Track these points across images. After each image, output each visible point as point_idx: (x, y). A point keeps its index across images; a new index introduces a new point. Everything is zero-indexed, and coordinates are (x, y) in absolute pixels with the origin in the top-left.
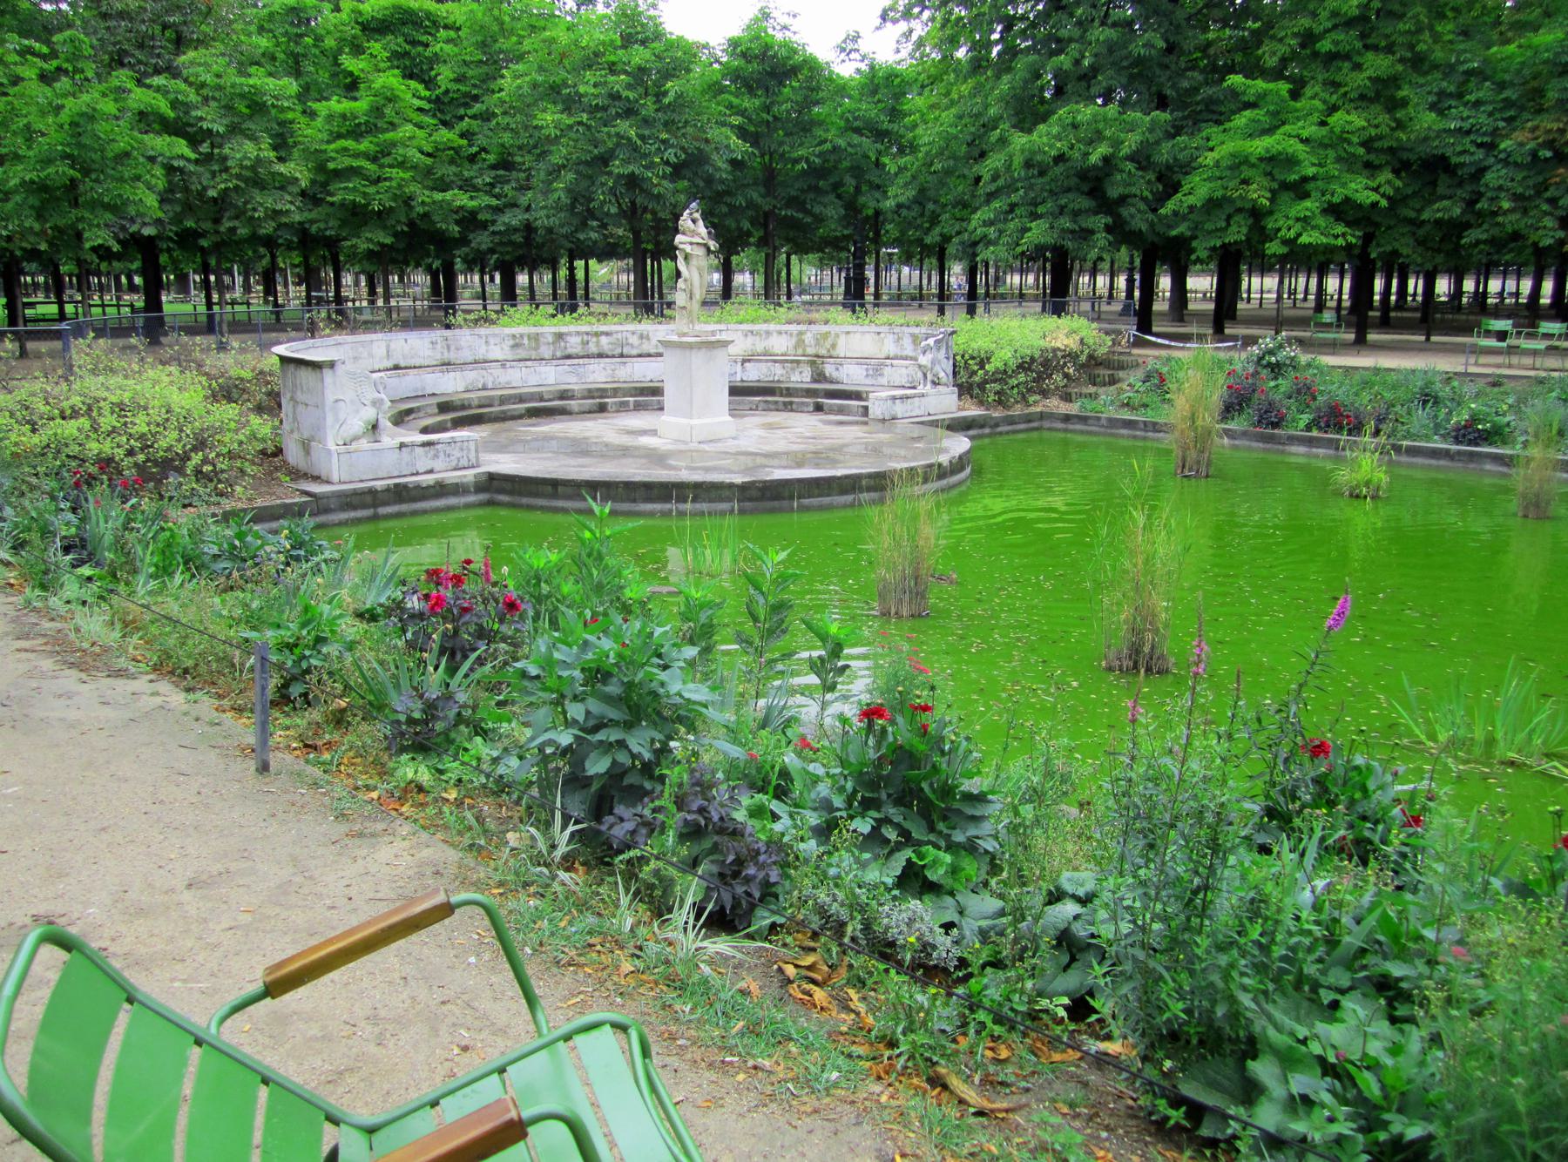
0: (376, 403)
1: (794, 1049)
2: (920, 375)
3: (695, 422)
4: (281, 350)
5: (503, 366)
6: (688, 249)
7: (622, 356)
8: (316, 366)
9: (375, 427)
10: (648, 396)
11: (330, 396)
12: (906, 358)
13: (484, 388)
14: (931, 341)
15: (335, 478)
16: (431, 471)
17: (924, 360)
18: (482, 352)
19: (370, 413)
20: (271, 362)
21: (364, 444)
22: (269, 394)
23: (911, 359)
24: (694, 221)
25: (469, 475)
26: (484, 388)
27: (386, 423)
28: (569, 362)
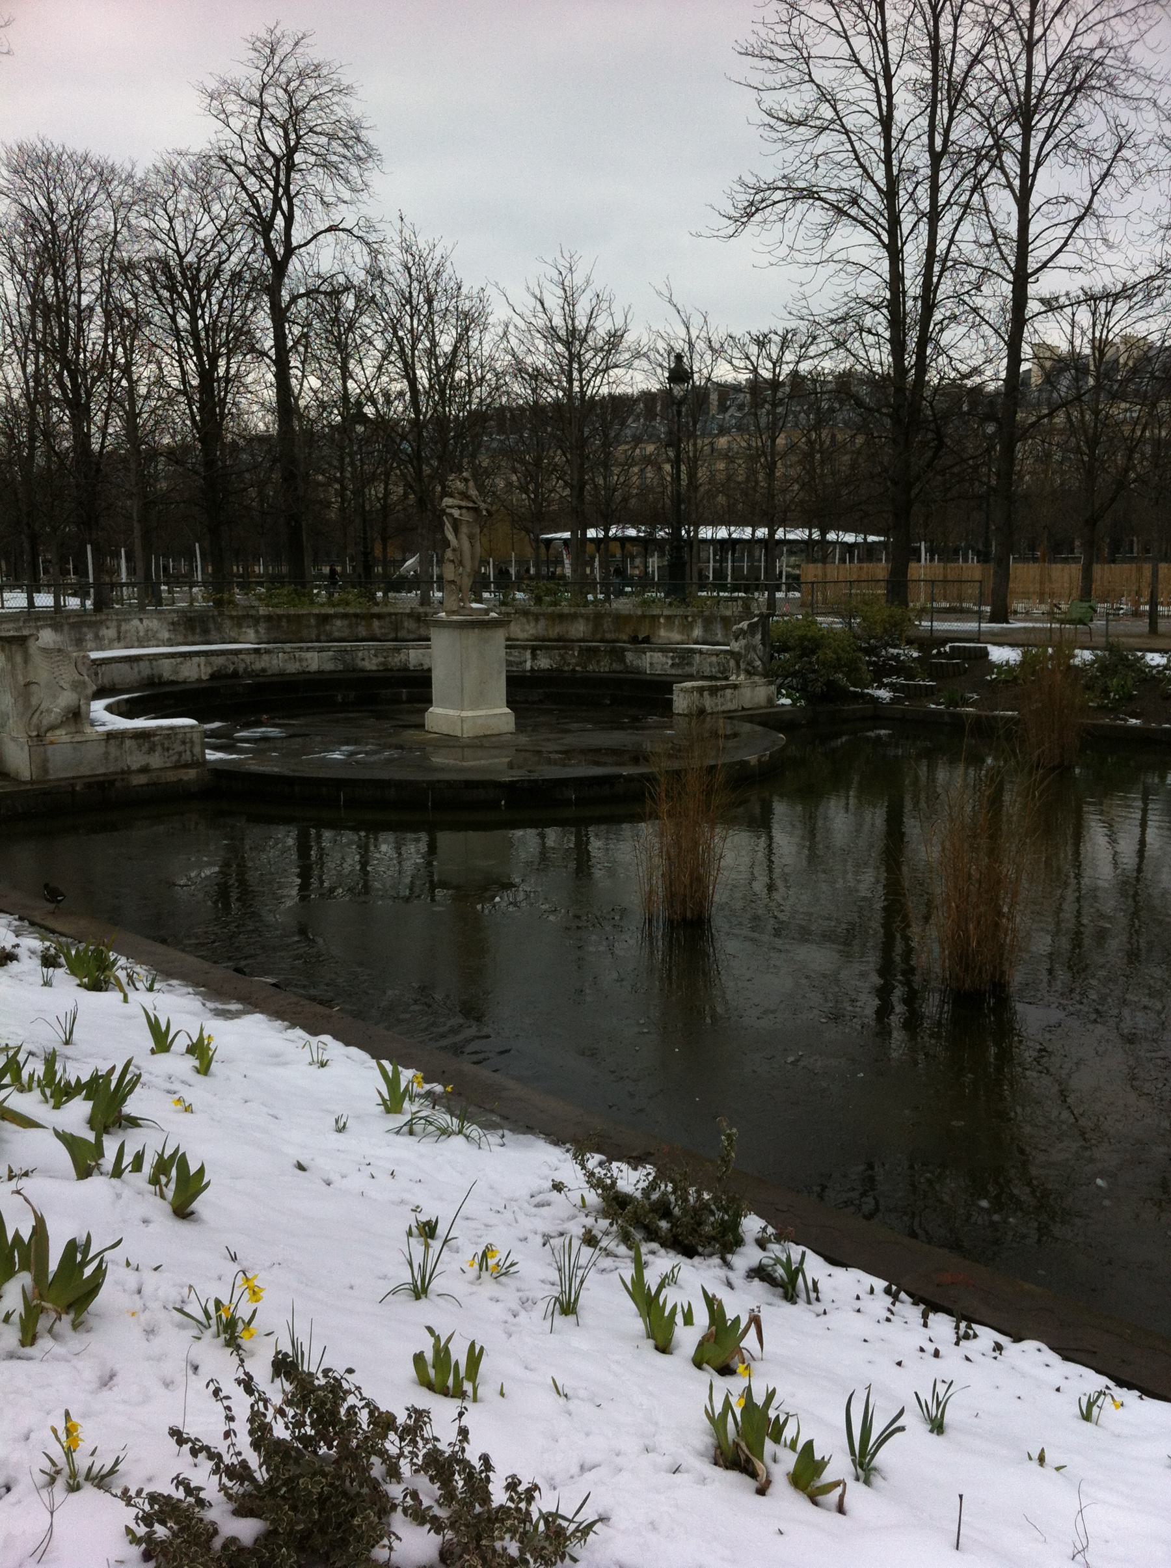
2: (732, 663)
3: (465, 714)
6: (456, 513)
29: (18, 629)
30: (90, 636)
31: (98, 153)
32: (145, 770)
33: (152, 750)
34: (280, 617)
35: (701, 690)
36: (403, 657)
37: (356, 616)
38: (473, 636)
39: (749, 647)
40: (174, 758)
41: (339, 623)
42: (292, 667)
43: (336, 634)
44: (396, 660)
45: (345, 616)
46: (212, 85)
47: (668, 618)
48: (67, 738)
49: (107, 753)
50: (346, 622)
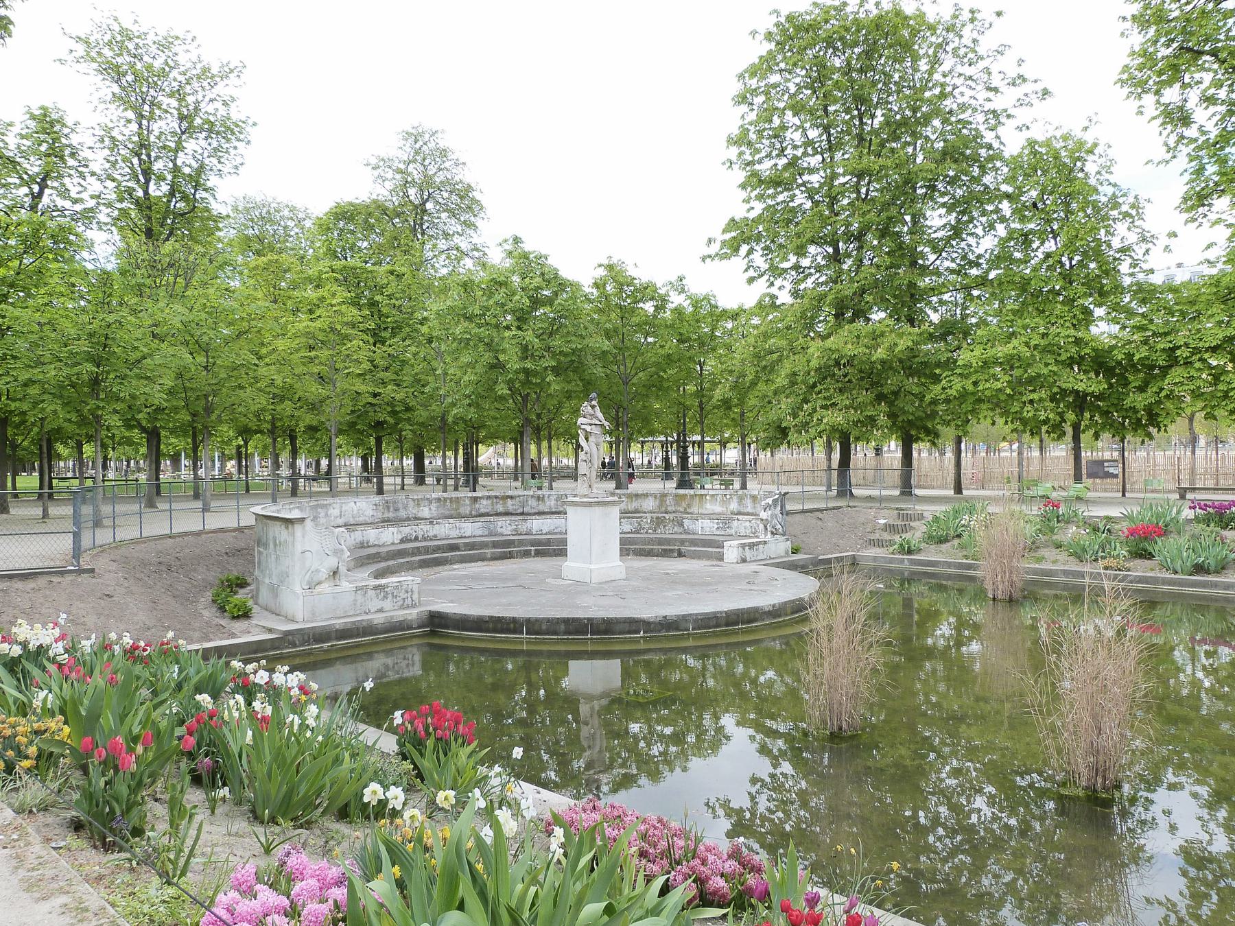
0: (338, 552)
1: (235, 284)
2: (761, 526)
3: (592, 567)
4: (258, 509)
5: (431, 523)
6: (588, 428)
7: (522, 514)
8: (288, 522)
9: (335, 573)
10: (553, 548)
11: (299, 548)
12: (748, 514)
13: (416, 539)
14: (770, 501)
15: (300, 617)
16: (381, 610)
17: (764, 515)
18: (413, 511)
19: (332, 562)
20: (248, 520)
21: (326, 588)
22: (1043, 311)
23: (752, 514)
24: (593, 407)
25: (412, 614)
26: (425, 539)
27: (343, 569)
28: (483, 519)
29: (278, 511)
30: (322, 515)
31: (299, 205)
32: (381, 610)
33: (385, 597)
34: (445, 499)
35: (743, 546)
36: (529, 524)
37: (496, 497)
38: (598, 510)
39: (774, 516)
40: (400, 603)
41: (484, 502)
42: (454, 534)
43: (483, 511)
44: (524, 527)
45: (489, 497)
46: (373, 161)
47: (713, 496)
48: (329, 590)
49: (355, 600)
50: (489, 502)
